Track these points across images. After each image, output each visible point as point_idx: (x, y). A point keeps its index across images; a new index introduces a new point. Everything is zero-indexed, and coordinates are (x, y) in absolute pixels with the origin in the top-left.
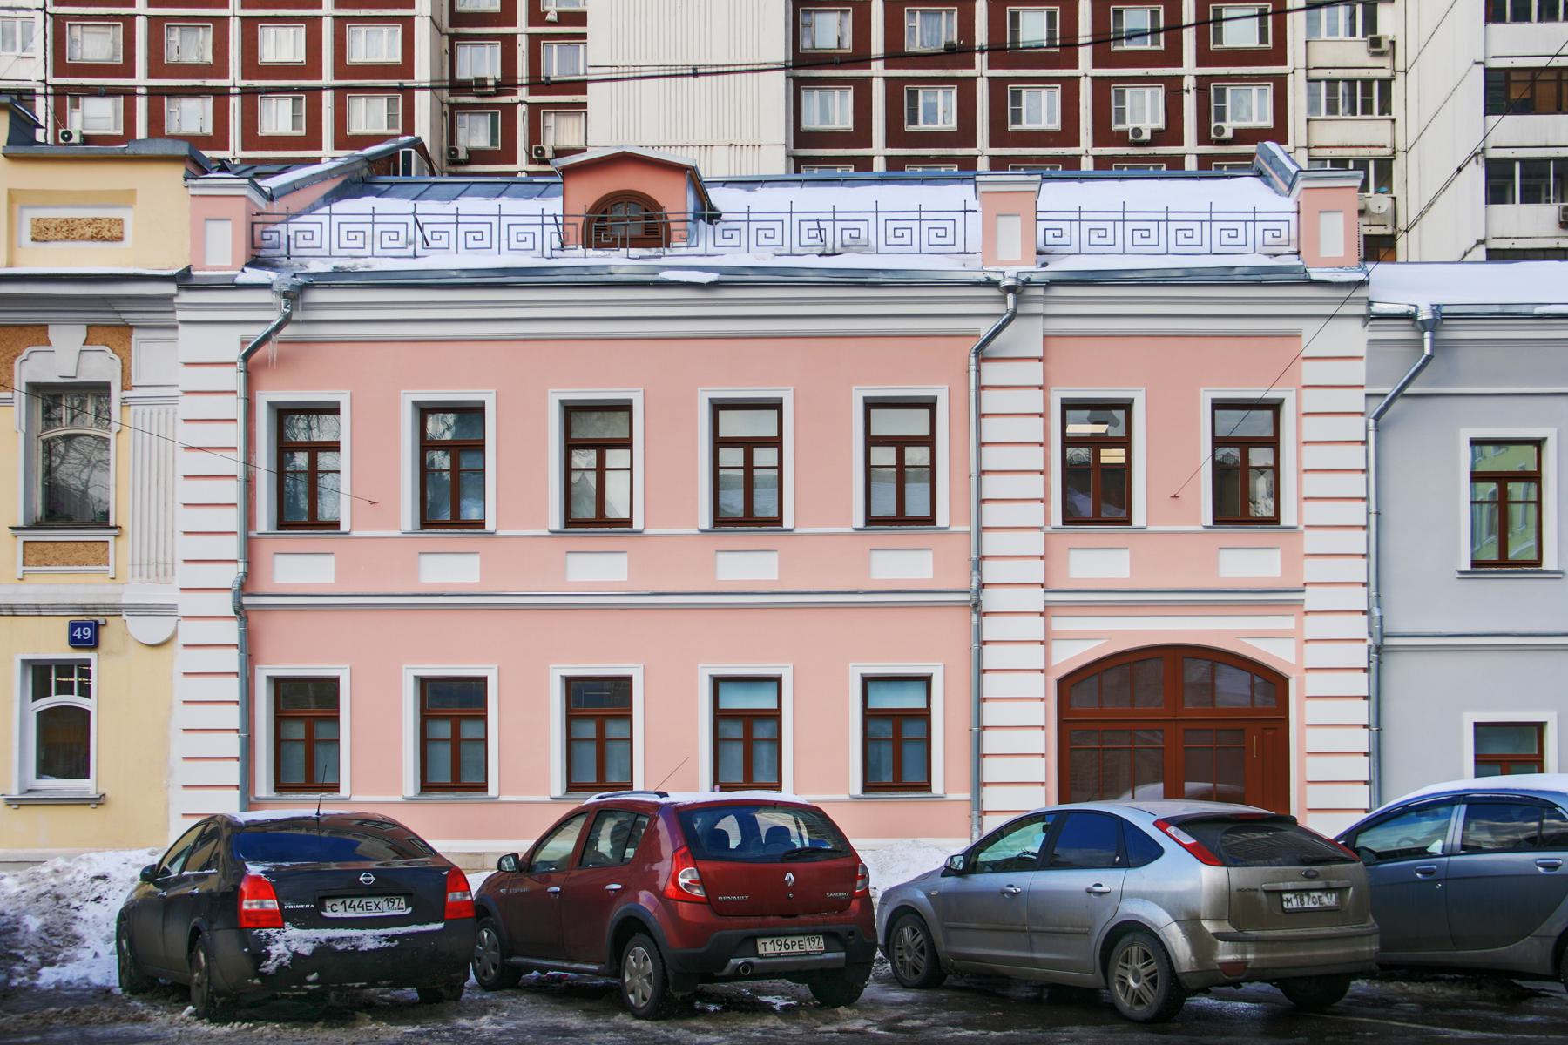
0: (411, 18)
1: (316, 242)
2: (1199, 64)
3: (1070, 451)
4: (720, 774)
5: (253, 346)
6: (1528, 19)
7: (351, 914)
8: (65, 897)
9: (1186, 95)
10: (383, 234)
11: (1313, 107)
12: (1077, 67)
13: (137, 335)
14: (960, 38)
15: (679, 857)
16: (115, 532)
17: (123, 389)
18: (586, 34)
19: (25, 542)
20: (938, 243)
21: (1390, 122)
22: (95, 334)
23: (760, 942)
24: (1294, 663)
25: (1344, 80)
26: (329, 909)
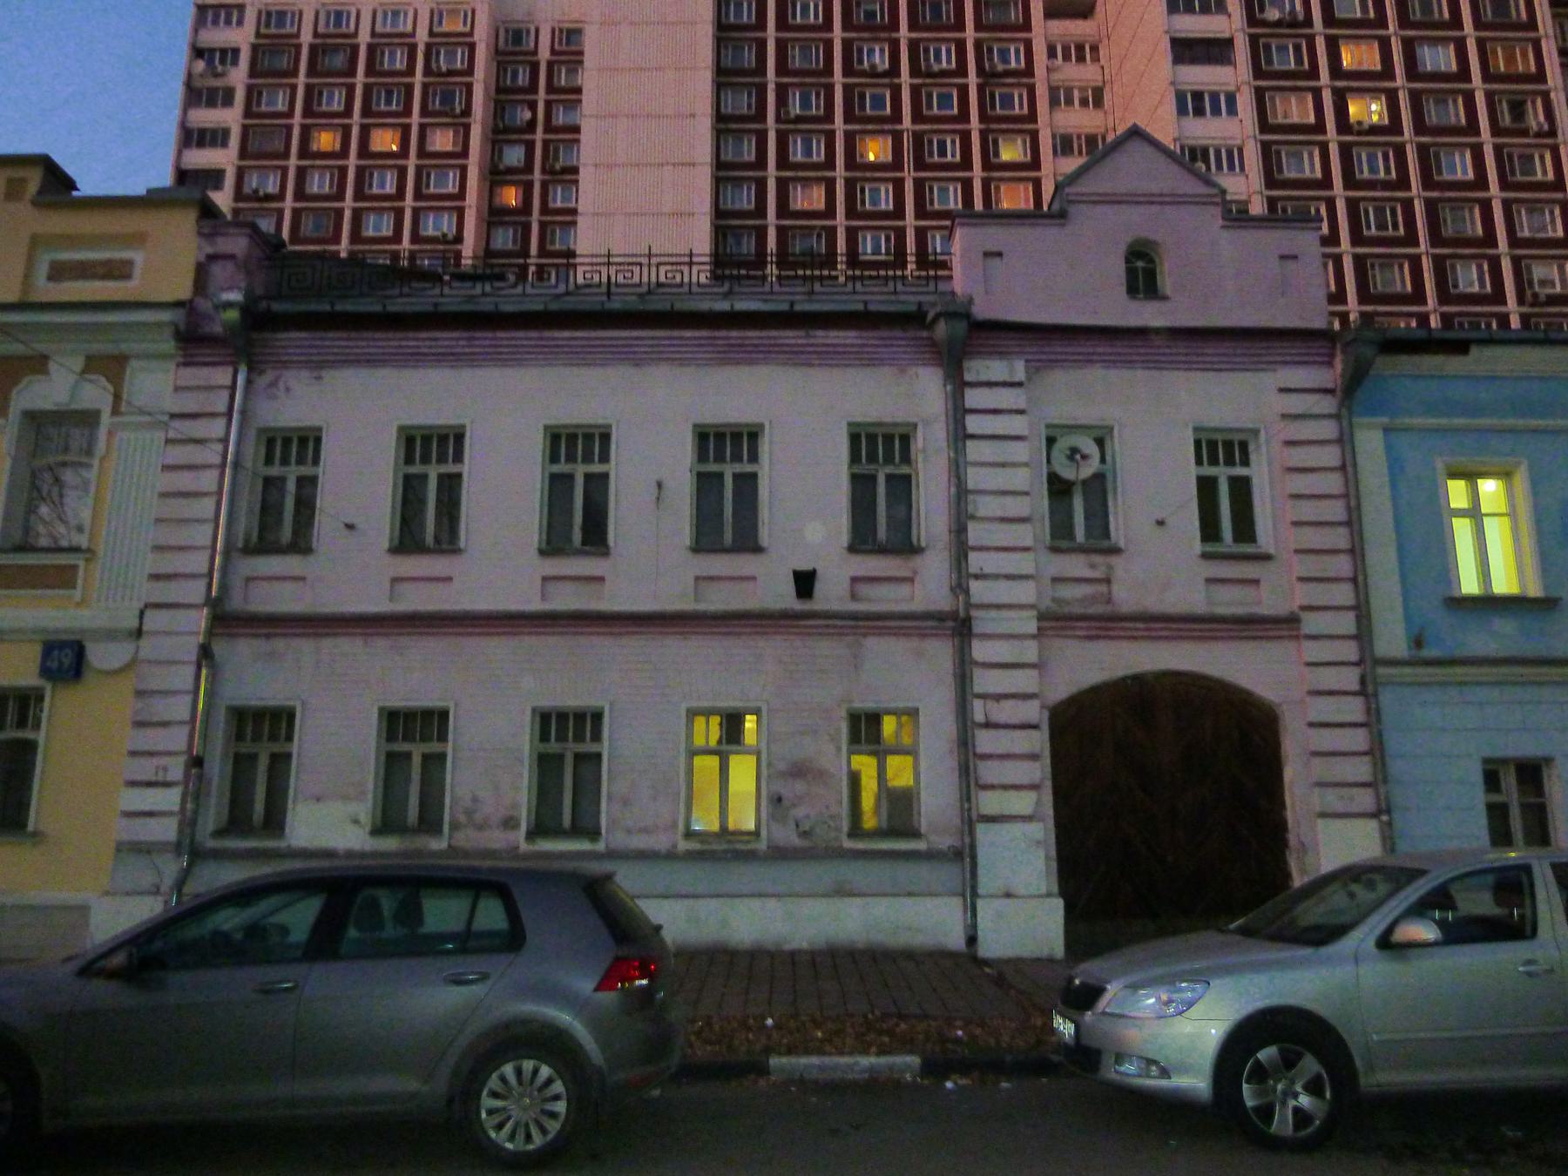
13: (134, 363)
15: (539, 284)
16: (87, 556)
18: (1178, 59)
22: (94, 365)
23: (755, 717)
24: (1454, 519)
25: (196, 31)
26: (438, 225)
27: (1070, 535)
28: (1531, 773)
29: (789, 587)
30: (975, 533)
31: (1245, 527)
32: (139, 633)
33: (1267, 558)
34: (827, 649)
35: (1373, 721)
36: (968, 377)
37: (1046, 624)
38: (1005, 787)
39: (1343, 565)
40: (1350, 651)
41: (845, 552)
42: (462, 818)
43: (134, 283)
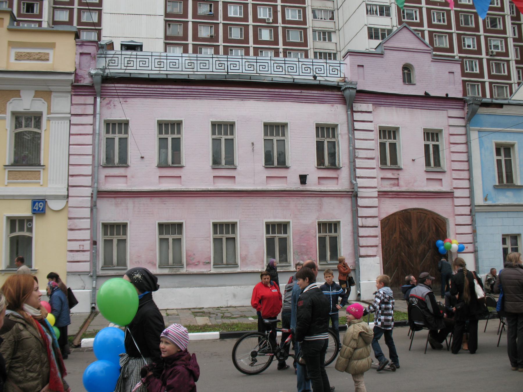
0: (41, 21)
1: (266, 69)
2: (79, 5)
3: (95, 20)
5: (400, 149)
6: (517, 248)
7: (231, 167)
8: (419, 350)
9: (280, 54)
11: (314, 39)
12: (249, 44)
13: (53, 94)
14: (214, 34)
17: (48, 114)
19: (9, 171)
27: (323, 164)
28: (515, 238)
29: (298, 180)
30: (359, 163)
31: (437, 163)
32: (68, 196)
33: (444, 172)
34: (313, 201)
35: (473, 224)
36: (354, 109)
37: (380, 193)
39: (465, 175)
40: (467, 202)
43: (50, 62)
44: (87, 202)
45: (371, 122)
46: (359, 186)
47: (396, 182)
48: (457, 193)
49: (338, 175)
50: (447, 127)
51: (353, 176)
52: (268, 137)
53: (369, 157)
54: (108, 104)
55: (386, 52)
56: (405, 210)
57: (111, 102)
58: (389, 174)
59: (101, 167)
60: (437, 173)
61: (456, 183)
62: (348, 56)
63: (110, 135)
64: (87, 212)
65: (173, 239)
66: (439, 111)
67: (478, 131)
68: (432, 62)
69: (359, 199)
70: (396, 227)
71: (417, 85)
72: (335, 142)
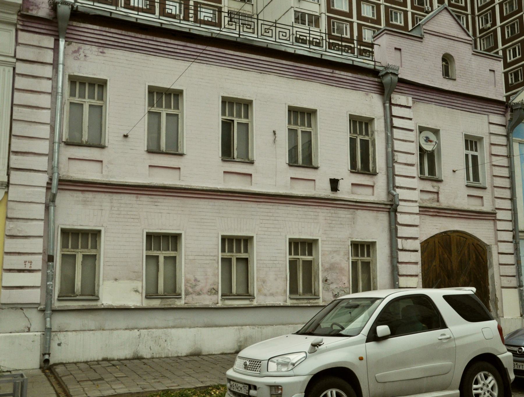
4: (504, 252)
10: (175, 7)
20: (225, 21)
21: (318, 5)
27: (296, 161)
29: (328, 186)
33: (485, 188)
34: (344, 214)
36: (393, 102)
38: (407, 276)
41: (287, 166)
42: (190, 290)
44: (41, 195)
45: (411, 119)
46: (400, 198)
47: (435, 196)
48: (500, 215)
49: (374, 183)
50: (488, 134)
51: (391, 185)
52: (291, 126)
53: (409, 162)
54: (75, 52)
55: (426, 36)
56: (445, 232)
57: (80, 50)
58: (428, 186)
59: (63, 144)
60: (477, 189)
61: (500, 204)
62: (383, 35)
63: (76, 99)
64: (39, 211)
65: (165, 257)
66: (479, 114)
67: (519, 143)
68: (472, 55)
69: (398, 215)
70: (435, 253)
71: (457, 81)
72: (368, 141)
